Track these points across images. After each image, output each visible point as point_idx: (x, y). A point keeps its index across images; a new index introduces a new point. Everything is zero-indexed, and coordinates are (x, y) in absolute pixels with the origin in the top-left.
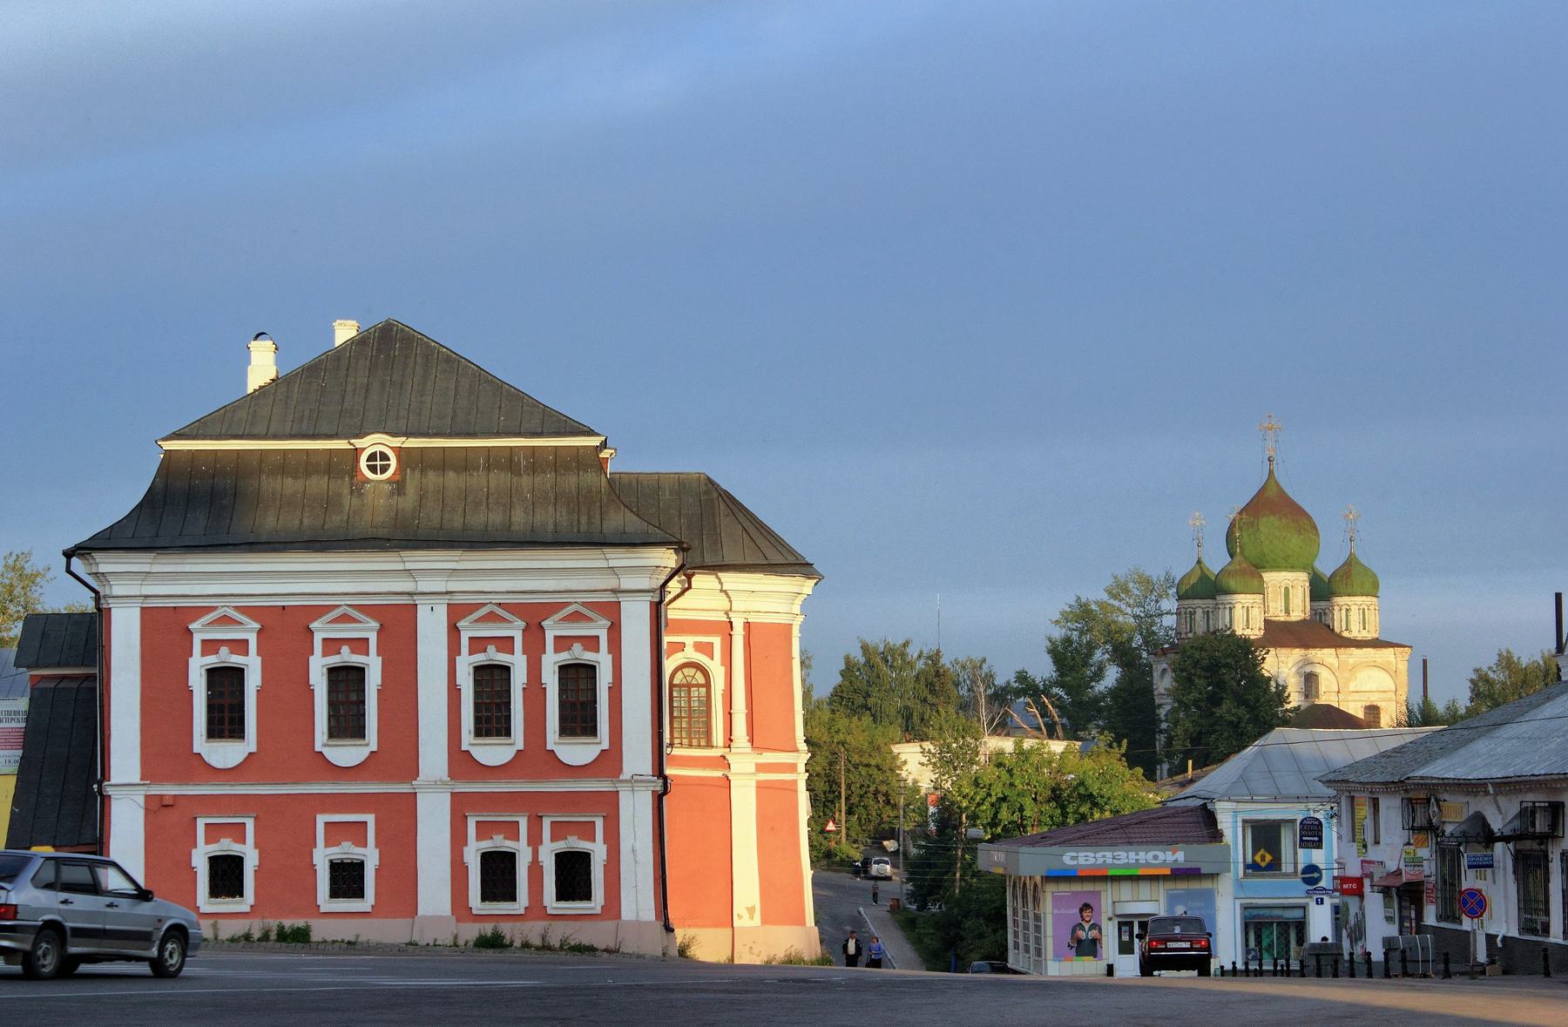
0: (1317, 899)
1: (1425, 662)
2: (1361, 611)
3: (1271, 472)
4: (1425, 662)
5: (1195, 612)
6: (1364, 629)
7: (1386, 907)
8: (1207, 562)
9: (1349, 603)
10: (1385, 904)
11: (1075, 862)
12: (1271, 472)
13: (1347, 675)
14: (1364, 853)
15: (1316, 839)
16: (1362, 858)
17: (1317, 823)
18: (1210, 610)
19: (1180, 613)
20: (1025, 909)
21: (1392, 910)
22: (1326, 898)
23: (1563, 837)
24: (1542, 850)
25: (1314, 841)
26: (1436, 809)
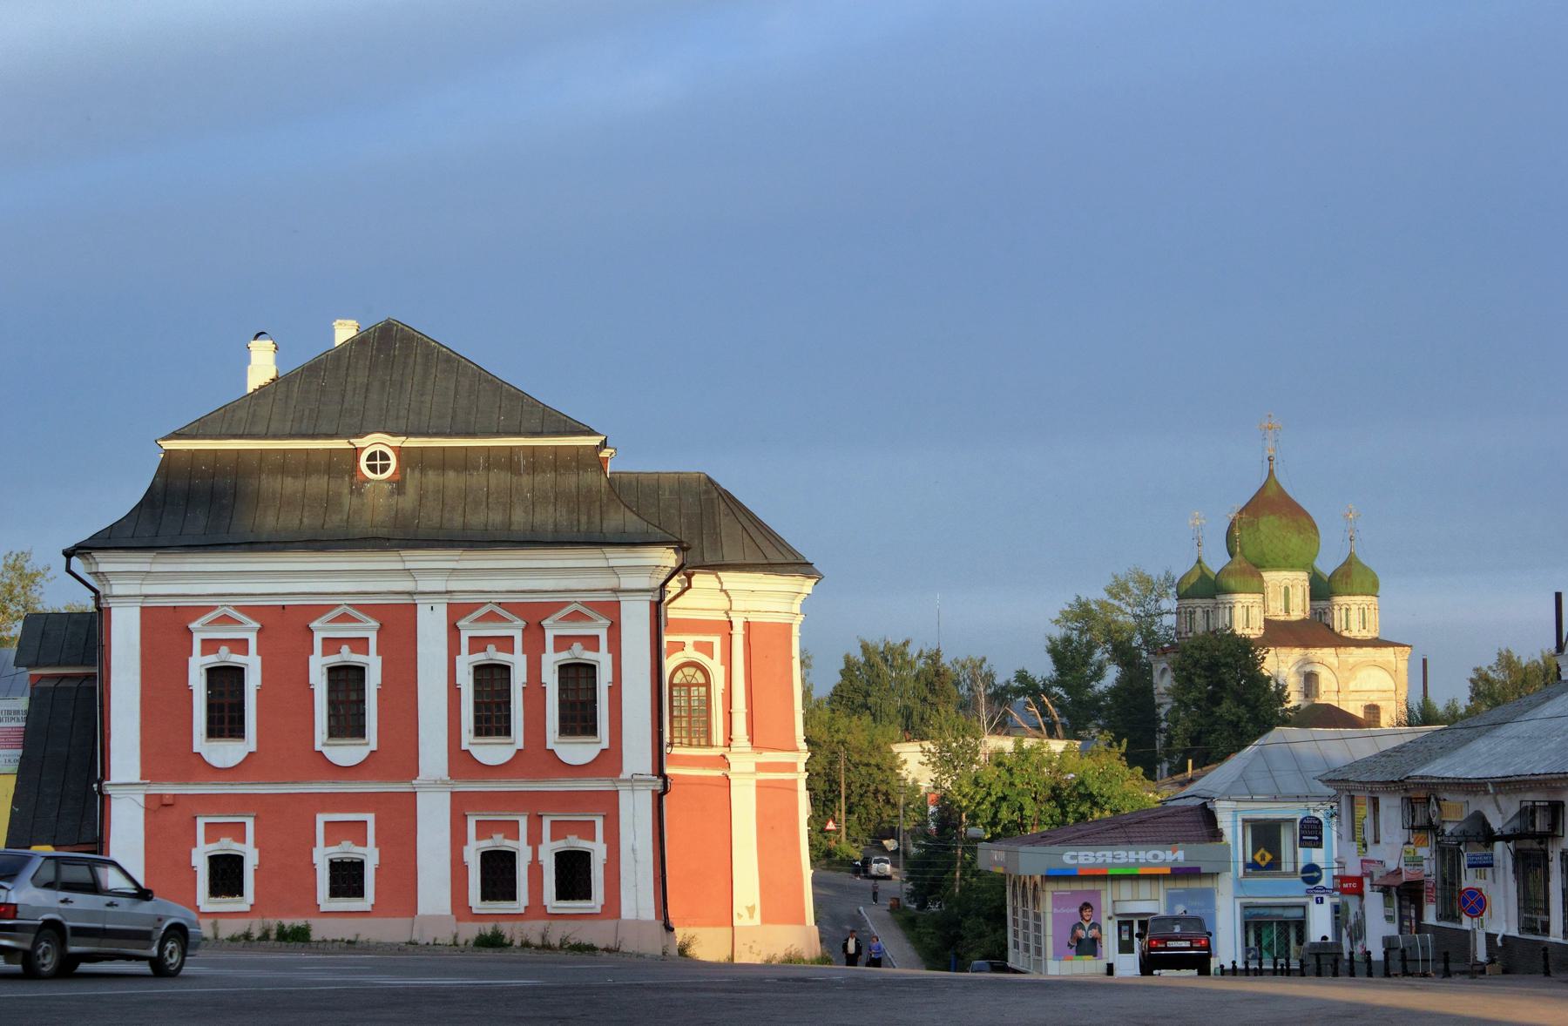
0: (1317, 898)
1: (1425, 661)
2: (1361, 611)
4: (1425, 661)
5: (1195, 612)
6: (1364, 628)
7: (1385, 906)
9: (1350, 603)
11: (1075, 862)
12: (1271, 472)
13: (1347, 674)
15: (1316, 838)
19: (1180, 613)
21: (1392, 909)
22: (1326, 898)
23: (1563, 836)
24: (1542, 850)
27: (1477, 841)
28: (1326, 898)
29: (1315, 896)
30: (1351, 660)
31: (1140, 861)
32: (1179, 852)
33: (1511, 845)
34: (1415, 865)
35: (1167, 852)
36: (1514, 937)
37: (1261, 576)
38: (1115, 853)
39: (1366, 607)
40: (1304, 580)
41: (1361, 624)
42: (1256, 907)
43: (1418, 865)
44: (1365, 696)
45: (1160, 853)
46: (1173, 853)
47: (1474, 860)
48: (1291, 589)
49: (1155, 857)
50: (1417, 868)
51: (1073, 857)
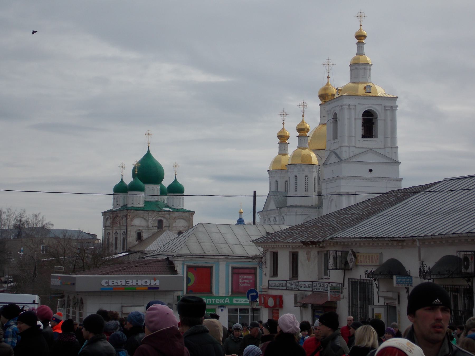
11: (107, 285)
24: (469, 286)
26: (353, 257)
30: (174, 216)
31: (139, 284)
34: (335, 292)
35: (151, 280)
43: (337, 292)
44: (178, 229)
45: (144, 284)
46: (154, 281)
49: (246, 277)
50: (337, 293)
51: (106, 282)
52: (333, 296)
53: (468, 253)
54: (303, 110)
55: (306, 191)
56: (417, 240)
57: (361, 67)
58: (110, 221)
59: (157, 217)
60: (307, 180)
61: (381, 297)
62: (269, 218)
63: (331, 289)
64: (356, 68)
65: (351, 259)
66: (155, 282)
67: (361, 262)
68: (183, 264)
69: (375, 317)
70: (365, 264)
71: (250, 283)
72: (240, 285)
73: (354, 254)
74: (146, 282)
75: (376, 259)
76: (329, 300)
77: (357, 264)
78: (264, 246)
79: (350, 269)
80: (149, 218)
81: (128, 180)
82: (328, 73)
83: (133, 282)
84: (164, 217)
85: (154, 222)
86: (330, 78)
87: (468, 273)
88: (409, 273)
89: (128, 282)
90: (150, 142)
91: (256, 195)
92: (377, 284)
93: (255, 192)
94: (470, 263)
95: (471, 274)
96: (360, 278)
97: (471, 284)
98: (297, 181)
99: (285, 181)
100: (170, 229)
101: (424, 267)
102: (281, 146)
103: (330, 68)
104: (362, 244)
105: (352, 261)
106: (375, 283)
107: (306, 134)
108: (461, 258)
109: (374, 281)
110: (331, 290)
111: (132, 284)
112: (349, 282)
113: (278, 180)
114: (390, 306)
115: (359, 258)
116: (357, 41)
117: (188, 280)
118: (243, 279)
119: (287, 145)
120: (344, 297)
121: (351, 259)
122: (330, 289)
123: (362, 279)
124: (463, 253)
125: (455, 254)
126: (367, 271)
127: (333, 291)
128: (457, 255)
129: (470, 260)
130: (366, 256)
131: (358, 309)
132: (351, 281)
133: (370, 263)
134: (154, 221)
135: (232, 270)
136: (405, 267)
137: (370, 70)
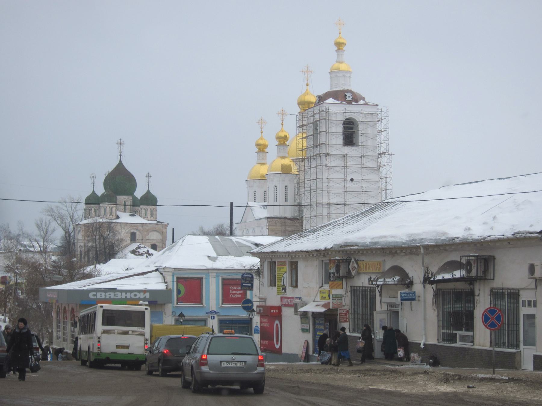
0: (211, 317)
1: (173, 229)
2: (151, 211)
3: (120, 160)
4: (173, 229)
5: (91, 209)
6: (152, 217)
7: (302, 323)
8: (96, 191)
9: (147, 207)
10: (301, 321)
11: (95, 297)
12: (120, 160)
13: (145, 233)
14: (284, 293)
15: (250, 285)
16: (282, 296)
17: (250, 276)
18: (97, 209)
19: (86, 210)
20: (65, 320)
21: (308, 325)
22: (216, 316)
23: (494, 279)
24: (471, 289)
25: (249, 286)
26: (356, 265)
27: (402, 284)
28: (216, 316)
29: (211, 315)
32: (147, 293)
33: (434, 286)
34: (338, 299)
36: (434, 345)
37: (117, 197)
38: (115, 293)
39: (153, 210)
40: (131, 199)
41: (151, 215)
42: (496, 337)
43: (340, 300)
44: (151, 242)
47: (405, 296)
48: (126, 202)
50: (339, 301)
51: (94, 295)
52: (335, 303)
53: (471, 258)
54: (282, 118)
55: (285, 201)
56: (421, 247)
57: (341, 74)
58: (81, 234)
59: (129, 229)
60: (276, 190)
61: (384, 303)
62: (248, 230)
63: (333, 297)
64: (336, 76)
65: (353, 267)
66: (144, 296)
67: (364, 270)
68: (173, 276)
69: (358, 332)
70: (368, 271)
71: (240, 294)
72: (231, 296)
73: (357, 261)
74: (135, 295)
75: (379, 266)
76: (332, 308)
77: (361, 272)
78: (262, 256)
79: (352, 277)
80: (122, 231)
81: (100, 191)
82: (307, 80)
83: (121, 295)
84: (137, 229)
85: (127, 234)
86: (309, 86)
87: (471, 277)
88: (412, 279)
89: (116, 295)
90: (122, 151)
91: (233, 206)
92: (380, 291)
93: (232, 203)
94: (473, 267)
95: (473, 277)
96: (362, 286)
97: (472, 287)
98: (277, 191)
99: (264, 191)
100: (143, 241)
101: (429, 273)
102: (259, 155)
103: (309, 75)
104: (365, 252)
105: (355, 270)
106: (378, 290)
107: (285, 142)
108: (465, 263)
109: (376, 287)
110: (334, 297)
111: (131, 294)
112: (351, 290)
113: (256, 191)
114: (392, 311)
115: (362, 266)
116: (336, 48)
117: (179, 292)
118: (233, 290)
119: (266, 154)
120: (345, 304)
121: (353, 267)
122: (333, 297)
123: (364, 287)
124: (466, 258)
125: (458, 260)
126: (371, 278)
127: (335, 298)
128: (461, 260)
129: (473, 264)
130: (369, 264)
131: (360, 315)
132: (353, 289)
133: (373, 270)
134: (126, 234)
135: (222, 281)
136: (408, 273)
137: (350, 77)
